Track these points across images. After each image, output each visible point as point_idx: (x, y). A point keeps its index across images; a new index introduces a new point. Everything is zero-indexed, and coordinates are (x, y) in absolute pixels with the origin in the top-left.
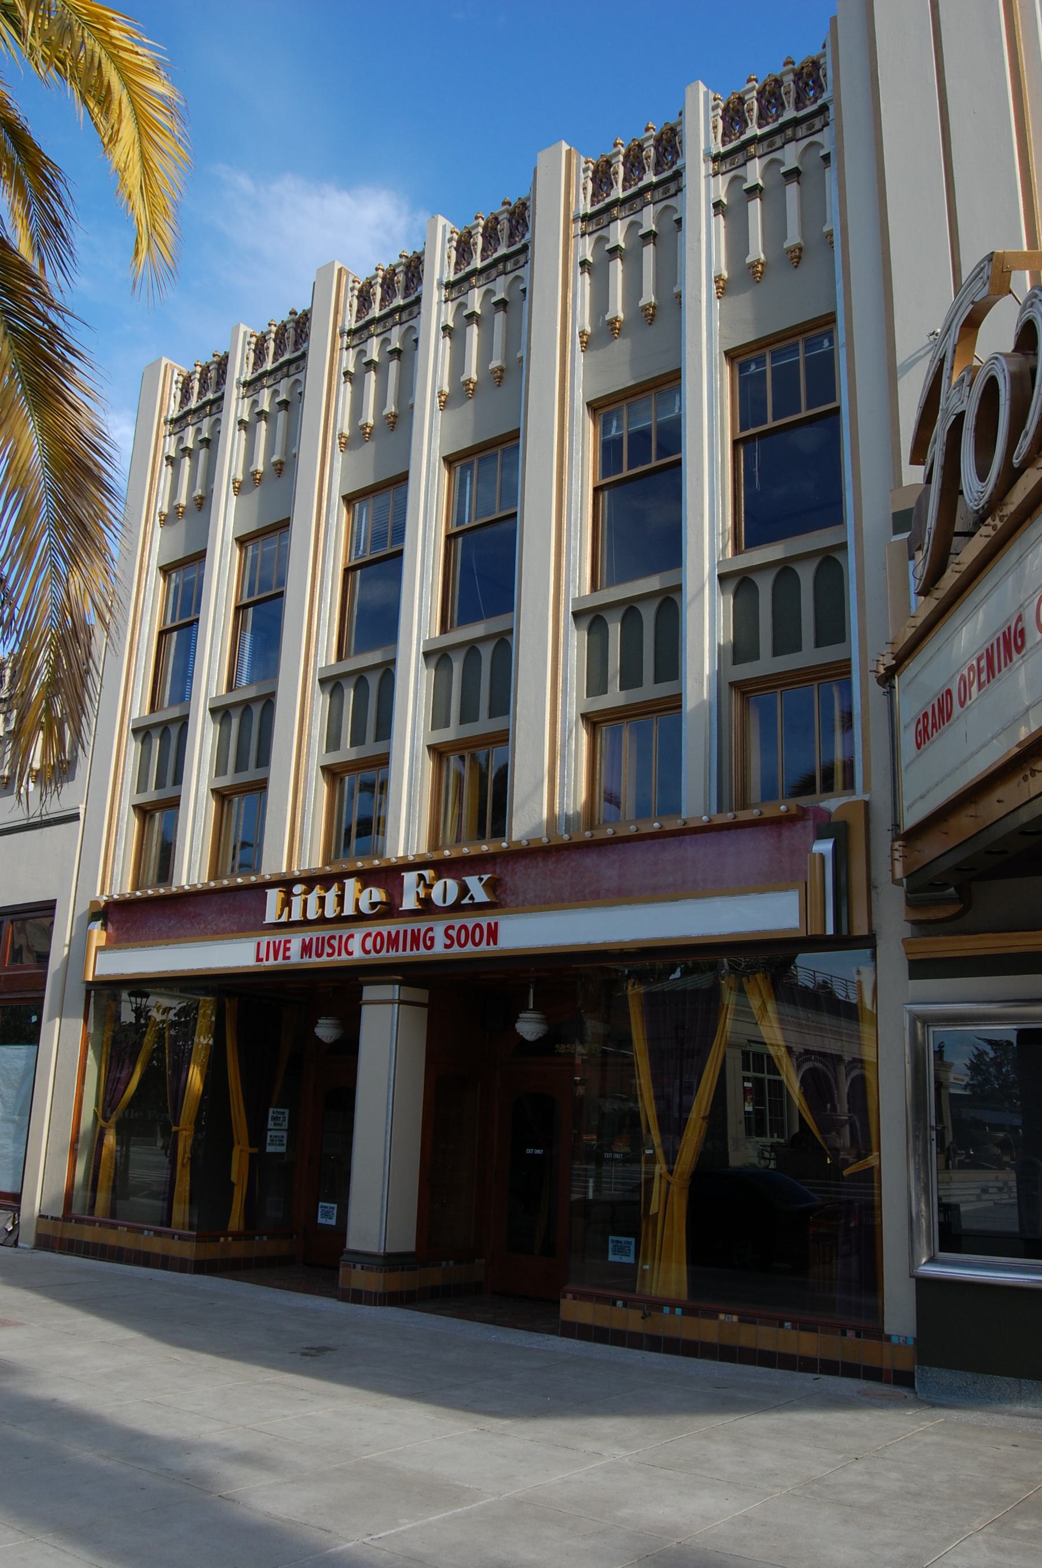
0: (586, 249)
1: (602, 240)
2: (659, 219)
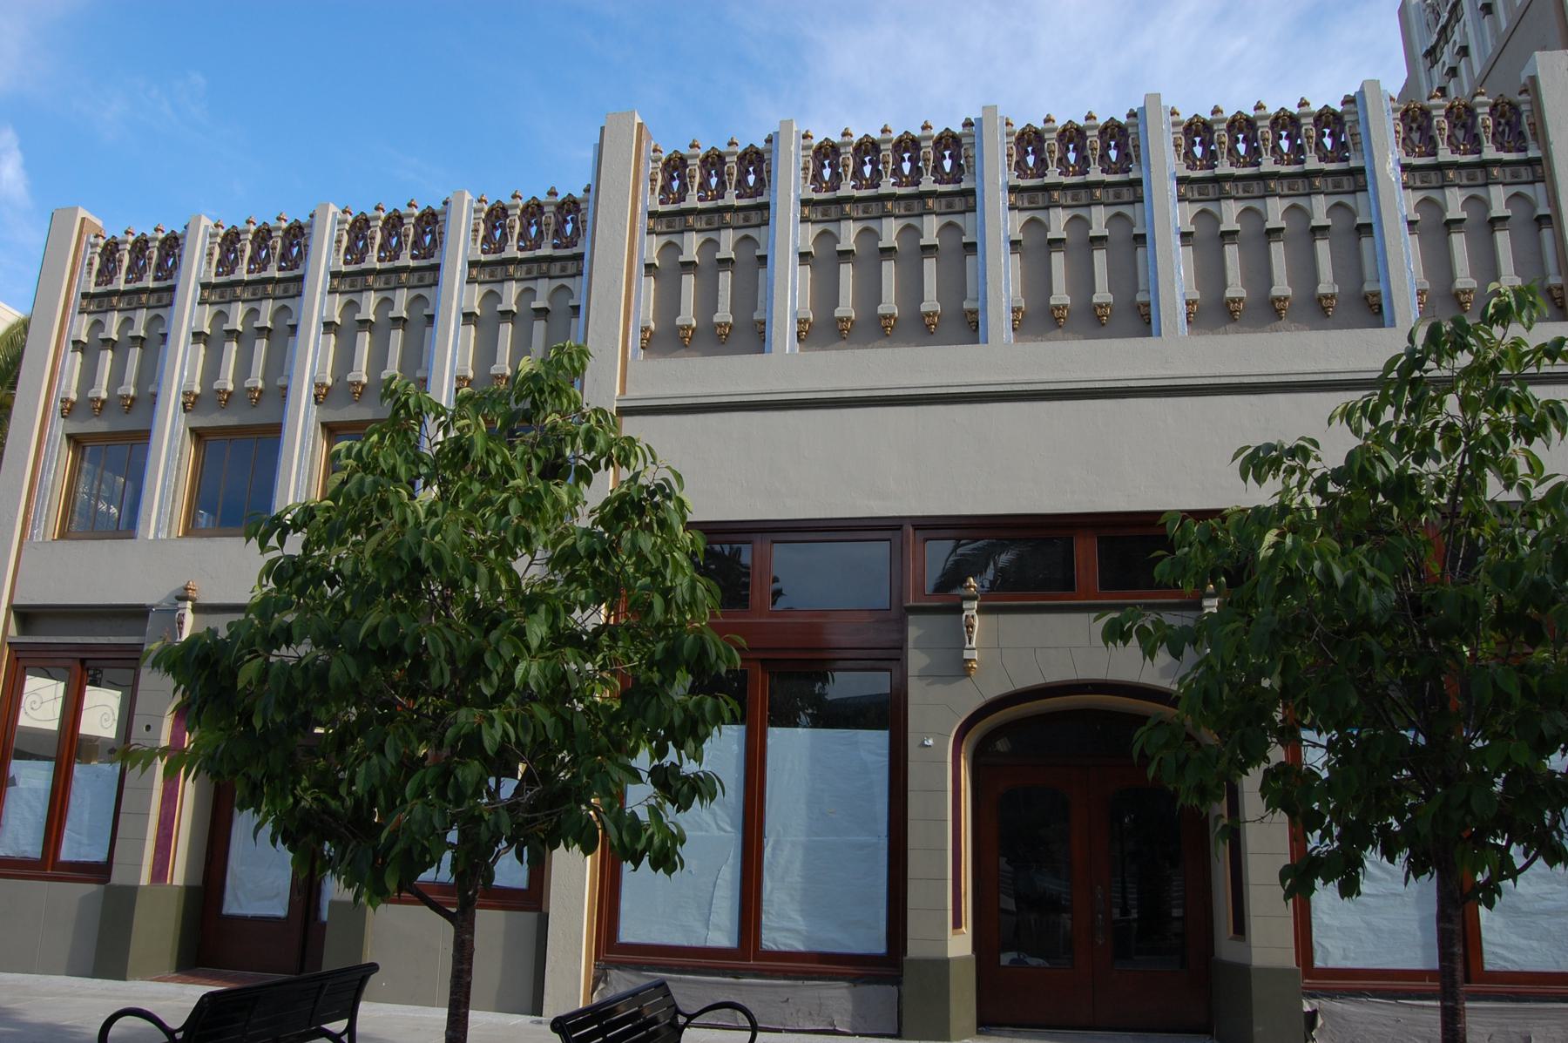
0: (651, 248)
1: (671, 248)
2: (149, 326)
